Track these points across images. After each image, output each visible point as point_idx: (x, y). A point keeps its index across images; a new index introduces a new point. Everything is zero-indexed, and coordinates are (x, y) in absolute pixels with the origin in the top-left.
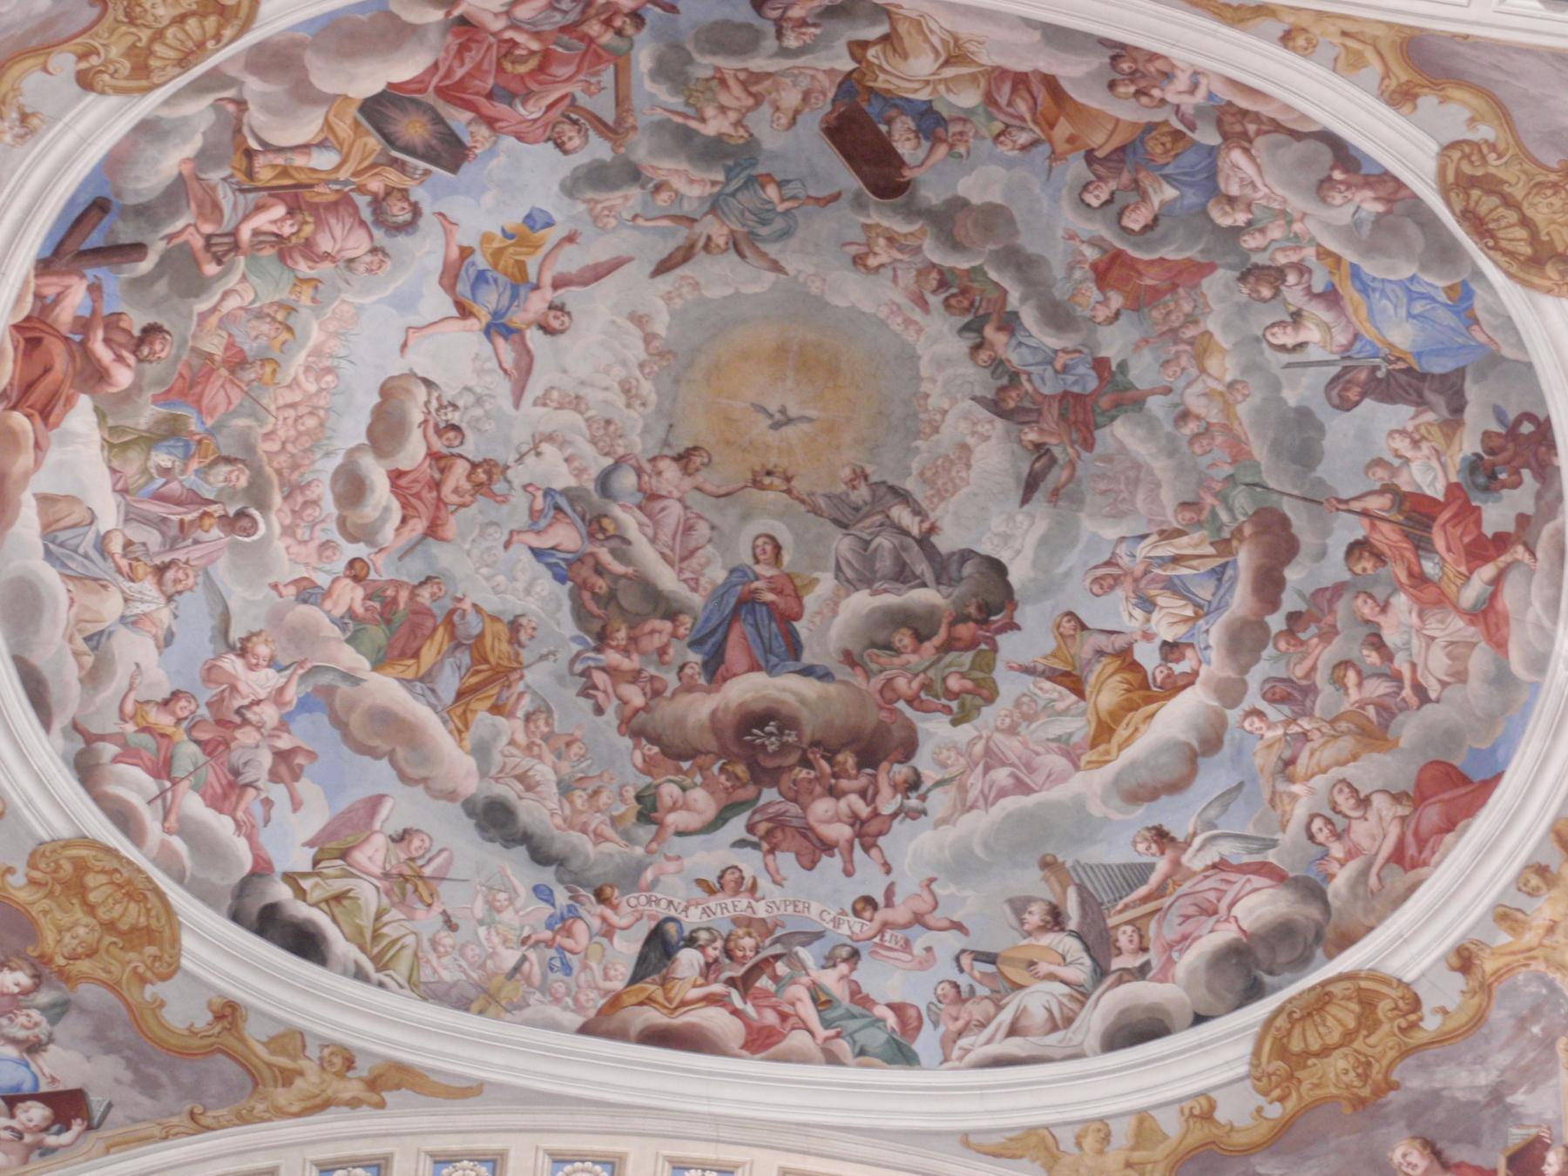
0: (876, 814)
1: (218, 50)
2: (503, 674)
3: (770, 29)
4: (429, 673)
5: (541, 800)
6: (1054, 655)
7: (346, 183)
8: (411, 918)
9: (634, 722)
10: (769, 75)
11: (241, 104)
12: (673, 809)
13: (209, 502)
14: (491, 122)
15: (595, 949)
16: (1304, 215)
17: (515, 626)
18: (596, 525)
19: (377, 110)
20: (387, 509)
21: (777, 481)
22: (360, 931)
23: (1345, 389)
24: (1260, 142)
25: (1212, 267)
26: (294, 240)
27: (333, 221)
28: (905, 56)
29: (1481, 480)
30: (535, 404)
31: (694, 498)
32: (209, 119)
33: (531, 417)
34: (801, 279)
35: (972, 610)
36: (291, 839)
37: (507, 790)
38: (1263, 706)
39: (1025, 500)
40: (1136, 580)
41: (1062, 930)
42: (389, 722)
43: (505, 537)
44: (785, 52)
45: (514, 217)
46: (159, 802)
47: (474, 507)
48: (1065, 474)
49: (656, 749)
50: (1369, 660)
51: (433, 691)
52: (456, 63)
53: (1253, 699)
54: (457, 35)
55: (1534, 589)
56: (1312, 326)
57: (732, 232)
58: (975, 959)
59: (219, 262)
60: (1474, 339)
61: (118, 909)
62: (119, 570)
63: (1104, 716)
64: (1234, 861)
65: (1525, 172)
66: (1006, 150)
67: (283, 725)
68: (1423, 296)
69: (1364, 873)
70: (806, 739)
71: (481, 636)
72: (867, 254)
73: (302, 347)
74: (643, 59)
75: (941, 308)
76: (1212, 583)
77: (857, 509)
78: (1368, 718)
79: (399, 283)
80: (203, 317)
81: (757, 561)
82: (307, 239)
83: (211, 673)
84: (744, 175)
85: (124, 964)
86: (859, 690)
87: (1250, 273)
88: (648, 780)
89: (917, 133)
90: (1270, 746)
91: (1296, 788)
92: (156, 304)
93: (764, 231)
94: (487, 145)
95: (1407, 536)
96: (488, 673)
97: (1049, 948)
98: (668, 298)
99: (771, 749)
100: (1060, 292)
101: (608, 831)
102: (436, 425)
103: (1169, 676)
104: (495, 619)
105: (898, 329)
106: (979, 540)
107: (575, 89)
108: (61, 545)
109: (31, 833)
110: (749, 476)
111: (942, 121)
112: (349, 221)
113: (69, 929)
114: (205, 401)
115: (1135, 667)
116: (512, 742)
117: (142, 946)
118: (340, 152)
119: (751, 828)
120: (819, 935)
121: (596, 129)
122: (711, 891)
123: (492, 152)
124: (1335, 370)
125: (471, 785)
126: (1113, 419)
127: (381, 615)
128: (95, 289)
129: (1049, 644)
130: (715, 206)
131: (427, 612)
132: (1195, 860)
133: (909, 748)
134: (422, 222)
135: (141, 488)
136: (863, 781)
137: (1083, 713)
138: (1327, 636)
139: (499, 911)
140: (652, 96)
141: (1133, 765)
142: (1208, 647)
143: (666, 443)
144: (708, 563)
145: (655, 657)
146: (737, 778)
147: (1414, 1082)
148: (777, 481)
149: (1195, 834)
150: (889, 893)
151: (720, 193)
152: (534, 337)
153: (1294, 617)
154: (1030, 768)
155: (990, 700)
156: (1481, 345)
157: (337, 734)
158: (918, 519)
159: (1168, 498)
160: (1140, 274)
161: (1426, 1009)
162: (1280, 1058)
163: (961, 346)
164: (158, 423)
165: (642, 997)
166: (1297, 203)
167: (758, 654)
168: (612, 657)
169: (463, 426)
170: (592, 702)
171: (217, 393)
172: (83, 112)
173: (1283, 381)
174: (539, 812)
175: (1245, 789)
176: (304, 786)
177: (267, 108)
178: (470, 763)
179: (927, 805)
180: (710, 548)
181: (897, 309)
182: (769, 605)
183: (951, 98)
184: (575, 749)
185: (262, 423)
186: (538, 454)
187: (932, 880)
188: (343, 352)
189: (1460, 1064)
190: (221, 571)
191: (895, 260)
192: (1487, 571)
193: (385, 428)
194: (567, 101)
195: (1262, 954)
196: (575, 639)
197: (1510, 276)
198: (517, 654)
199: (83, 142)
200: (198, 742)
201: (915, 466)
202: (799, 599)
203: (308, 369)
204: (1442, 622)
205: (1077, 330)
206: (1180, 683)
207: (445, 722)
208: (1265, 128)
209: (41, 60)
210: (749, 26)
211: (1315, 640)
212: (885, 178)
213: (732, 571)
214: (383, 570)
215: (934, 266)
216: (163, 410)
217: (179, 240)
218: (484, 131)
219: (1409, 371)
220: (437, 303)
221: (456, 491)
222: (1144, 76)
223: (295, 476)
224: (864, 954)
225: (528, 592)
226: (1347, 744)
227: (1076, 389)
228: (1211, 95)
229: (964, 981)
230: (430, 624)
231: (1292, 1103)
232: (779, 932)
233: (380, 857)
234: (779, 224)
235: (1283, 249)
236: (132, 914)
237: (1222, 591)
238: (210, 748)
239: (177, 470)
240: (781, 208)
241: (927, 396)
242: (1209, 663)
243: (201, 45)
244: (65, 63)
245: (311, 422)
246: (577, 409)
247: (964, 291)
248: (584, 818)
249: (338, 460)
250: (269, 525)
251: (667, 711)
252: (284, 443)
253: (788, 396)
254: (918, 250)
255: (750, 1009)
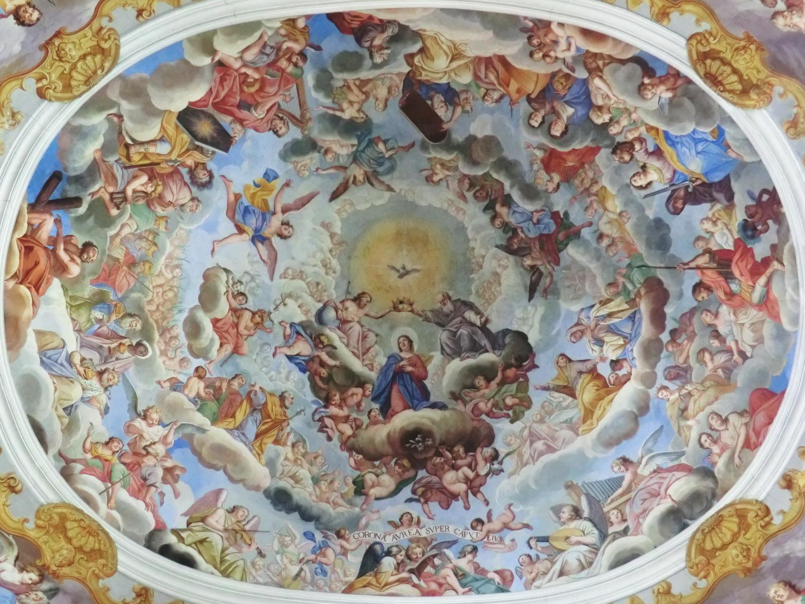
0: (478, 475)
1: (104, 76)
2: (279, 424)
3: (366, 53)
4: (241, 425)
5: (304, 488)
6: (557, 378)
7: (175, 161)
8: (240, 552)
9: (349, 443)
10: (369, 81)
11: (120, 117)
12: (373, 486)
13: (122, 338)
14: (241, 121)
15: (339, 562)
16: (636, 108)
17: (282, 397)
18: (317, 340)
19: (187, 117)
20: (212, 340)
21: (405, 306)
22: (214, 558)
23: (675, 202)
24: (606, 70)
25: (598, 149)
26: (153, 194)
27: (171, 184)
28: (433, 59)
29: (750, 233)
30: (281, 277)
31: (365, 320)
32: (105, 127)
33: (280, 285)
34: (403, 194)
35: (513, 361)
36: (175, 511)
37: (285, 484)
38: (666, 383)
39: (531, 298)
40: (592, 331)
41: (581, 518)
42: (220, 450)
43: (273, 350)
44: (376, 66)
45: (258, 177)
46: (105, 494)
47: (255, 337)
48: (548, 280)
49: (361, 456)
50: (714, 345)
51: (243, 434)
52: (220, 88)
53: (661, 381)
54: (219, 72)
55: (786, 282)
56: (652, 172)
57: (366, 172)
58: (538, 541)
59: (118, 208)
60: (730, 157)
61: (84, 540)
62: (79, 373)
63: (587, 406)
64: (665, 467)
65: (728, 44)
66: (489, 104)
67: (168, 454)
68: (701, 140)
69: (731, 458)
70: (438, 442)
71: (265, 404)
72: (432, 175)
73: (163, 254)
74: (309, 79)
75: (473, 199)
76: (630, 324)
77: (447, 315)
78: (719, 376)
79: (207, 216)
80: (113, 238)
81: (401, 350)
82: (160, 194)
83: (129, 428)
84: (367, 139)
85: (88, 569)
86: (461, 412)
87: (619, 148)
88: (358, 473)
89: (445, 102)
90: (673, 404)
91: (691, 422)
92: (89, 231)
93: (380, 169)
94: (241, 135)
95: (720, 274)
96: (270, 422)
97: (575, 528)
98: (338, 212)
99: (420, 449)
100: (528, 179)
101: (340, 501)
102: (233, 293)
103: (617, 378)
104: (272, 394)
105: (454, 214)
106: (511, 324)
107: (278, 99)
108: (49, 358)
109: (36, 500)
110: (391, 305)
111: (456, 94)
112: (179, 183)
113: (58, 551)
114: (117, 283)
115: (599, 377)
116: (286, 459)
117: (96, 559)
118: (170, 143)
119: (414, 492)
120: (455, 542)
121: (292, 122)
122: (396, 526)
123: (243, 139)
124: (668, 193)
125: (266, 481)
126: (566, 245)
127: (214, 396)
128: (58, 221)
129: (555, 372)
130: (355, 158)
131: (237, 393)
132: (645, 470)
133: (490, 438)
134: (214, 181)
135: (88, 329)
136: (469, 459)
137: (577, 406)
138: (691, 338)
139: (287, 547)
140: (317, 100)
141: (606, 428)
142: (633, 358)
143: (348, 292)
144: (377, 354)
145: (356, 408)
146: (404, 466)
147: (775, 554)
148: (405, 306)
149: (642, 457)
150: (489, 515)
151: (357, 151)
152: (276, 240)
153: (673, 333)
154: (554, 439)
155: (528, 407)
156: (734, 160)
157: (195, 458)
158: (478, 317)
159: (601, 283)
160: (565, 160)
161: (773, 512)
162: (703, 556)
163: (485, 219)
164: (94, 295)
165: (365, 583)
166: (631, 102)
167: (407, 399)
168: (334, 410)
169: (246, 293)
170: (325, 435)
171: (123, 279)
172: (42, 112)
173: (644, 205)
174: (303, 494)
175: (665, 428)
176: (181, 485)
177: (132, 119)
178: (266, 471)
179: (504, 466)
180: (376, 346)
181: (451, 203)
182: (409, 373)
183: (458, 79)
184: (319, 460)
185: (146, 295)
186: (285, 305)
187: (510, 505)
188: (182, 256)
189: (797, 538)
190: (131, 374)
191: (447, 176)
192: (762, 280)
193: (208, 297)
194: (276, 106)
195: (686, 511)
196: (313, 402)
197: (735, 104)
198: (285, 413)
199: (43, 129)
200: (124, 464)
201: (473, 288)
202: (425, 368)
203: (167, 266)
204: (746, 314)
205: (540, 199)
206: (623, 380)
207: (251, 450)
208: (606, 61)
209: (19, 82)
210: (356, 53)
211: (686, 342)
212: (435, 132)
213: (389, 358)
214: (213, 372)
215: (465, 176)
216: (96, 288)
217: (96, 197)
218: (238, 127)
219: (704, 184)
220: (226, 227)
221: (246, 328)
222: (545, 45)
223: (165, 323)
224: (480, 549)
225: (287, 379)
226: (711, 392)
227: (545, 232)
228: (578, 49)
229: (533, 553)
230: (239, 399)
231: (712, 578)
232: (434, 543)
233: (222, 521)
234: (387, 164)
235: (630, 131)
236: (91, 543)
237: (636, 326)
238: (131, 466)
239: (105, 320)
240: (387, 155)
241: (473, 249)
242: (635, 367)
243: (95, 73)
244: (30, 83)
245: (170, 295)
246: (302, 279)
247: (482, 188)
248: (327, 495)
249: (185, 314)
250: (154, 349)
251: (365, 436)
252: (158, 306)
253: (404, 260)
254: (456, 169)
255: (422, 583)
